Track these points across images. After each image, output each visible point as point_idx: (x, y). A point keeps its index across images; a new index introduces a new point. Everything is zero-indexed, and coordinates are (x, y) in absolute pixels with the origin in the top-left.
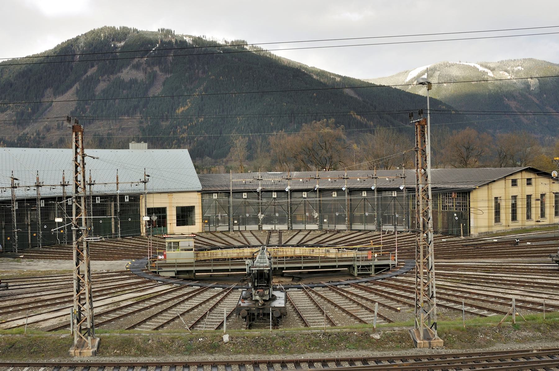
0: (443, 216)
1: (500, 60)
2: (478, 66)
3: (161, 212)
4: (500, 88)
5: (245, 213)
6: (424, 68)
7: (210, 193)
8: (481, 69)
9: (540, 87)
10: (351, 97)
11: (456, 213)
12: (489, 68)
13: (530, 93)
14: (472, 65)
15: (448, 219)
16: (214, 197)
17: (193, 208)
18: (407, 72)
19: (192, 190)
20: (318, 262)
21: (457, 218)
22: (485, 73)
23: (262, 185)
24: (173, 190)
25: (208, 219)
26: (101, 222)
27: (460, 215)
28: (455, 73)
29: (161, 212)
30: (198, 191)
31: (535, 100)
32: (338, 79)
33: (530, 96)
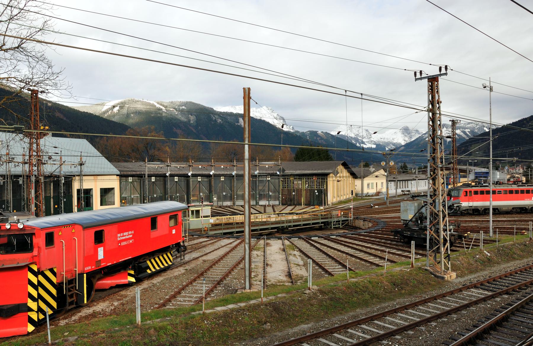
0: (306, 192)
1: (171, 101)
2: (156, 104)
3: (88, 192)
4: (171, 120)
5: (154, 194)
6: (120, 101)
7: (127, 176)
8: (158, 106)
9: (196, 122)
10: (62, 119)
11: (317, 190)
12: (163, 106)
13: (190, 125)
14: (152, 102)
15: (310, 195)
16: (130, 180)
17: (113, 189)
18: (103, 105)
19: (112, 173)
20: (234, 228)
21: (317, 194)
22: (160, 109)
23: (171, 171)
24: (111, 173)
25: (125, 198)
26: (222, 179)
27: (320, 191)
28: (140, 107)
29: (88, 192)
30: (117, 175)
31: (194, 130)
32: (50, 104)
33: (190, 127)
